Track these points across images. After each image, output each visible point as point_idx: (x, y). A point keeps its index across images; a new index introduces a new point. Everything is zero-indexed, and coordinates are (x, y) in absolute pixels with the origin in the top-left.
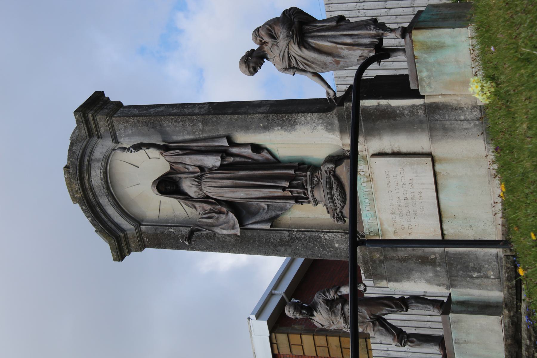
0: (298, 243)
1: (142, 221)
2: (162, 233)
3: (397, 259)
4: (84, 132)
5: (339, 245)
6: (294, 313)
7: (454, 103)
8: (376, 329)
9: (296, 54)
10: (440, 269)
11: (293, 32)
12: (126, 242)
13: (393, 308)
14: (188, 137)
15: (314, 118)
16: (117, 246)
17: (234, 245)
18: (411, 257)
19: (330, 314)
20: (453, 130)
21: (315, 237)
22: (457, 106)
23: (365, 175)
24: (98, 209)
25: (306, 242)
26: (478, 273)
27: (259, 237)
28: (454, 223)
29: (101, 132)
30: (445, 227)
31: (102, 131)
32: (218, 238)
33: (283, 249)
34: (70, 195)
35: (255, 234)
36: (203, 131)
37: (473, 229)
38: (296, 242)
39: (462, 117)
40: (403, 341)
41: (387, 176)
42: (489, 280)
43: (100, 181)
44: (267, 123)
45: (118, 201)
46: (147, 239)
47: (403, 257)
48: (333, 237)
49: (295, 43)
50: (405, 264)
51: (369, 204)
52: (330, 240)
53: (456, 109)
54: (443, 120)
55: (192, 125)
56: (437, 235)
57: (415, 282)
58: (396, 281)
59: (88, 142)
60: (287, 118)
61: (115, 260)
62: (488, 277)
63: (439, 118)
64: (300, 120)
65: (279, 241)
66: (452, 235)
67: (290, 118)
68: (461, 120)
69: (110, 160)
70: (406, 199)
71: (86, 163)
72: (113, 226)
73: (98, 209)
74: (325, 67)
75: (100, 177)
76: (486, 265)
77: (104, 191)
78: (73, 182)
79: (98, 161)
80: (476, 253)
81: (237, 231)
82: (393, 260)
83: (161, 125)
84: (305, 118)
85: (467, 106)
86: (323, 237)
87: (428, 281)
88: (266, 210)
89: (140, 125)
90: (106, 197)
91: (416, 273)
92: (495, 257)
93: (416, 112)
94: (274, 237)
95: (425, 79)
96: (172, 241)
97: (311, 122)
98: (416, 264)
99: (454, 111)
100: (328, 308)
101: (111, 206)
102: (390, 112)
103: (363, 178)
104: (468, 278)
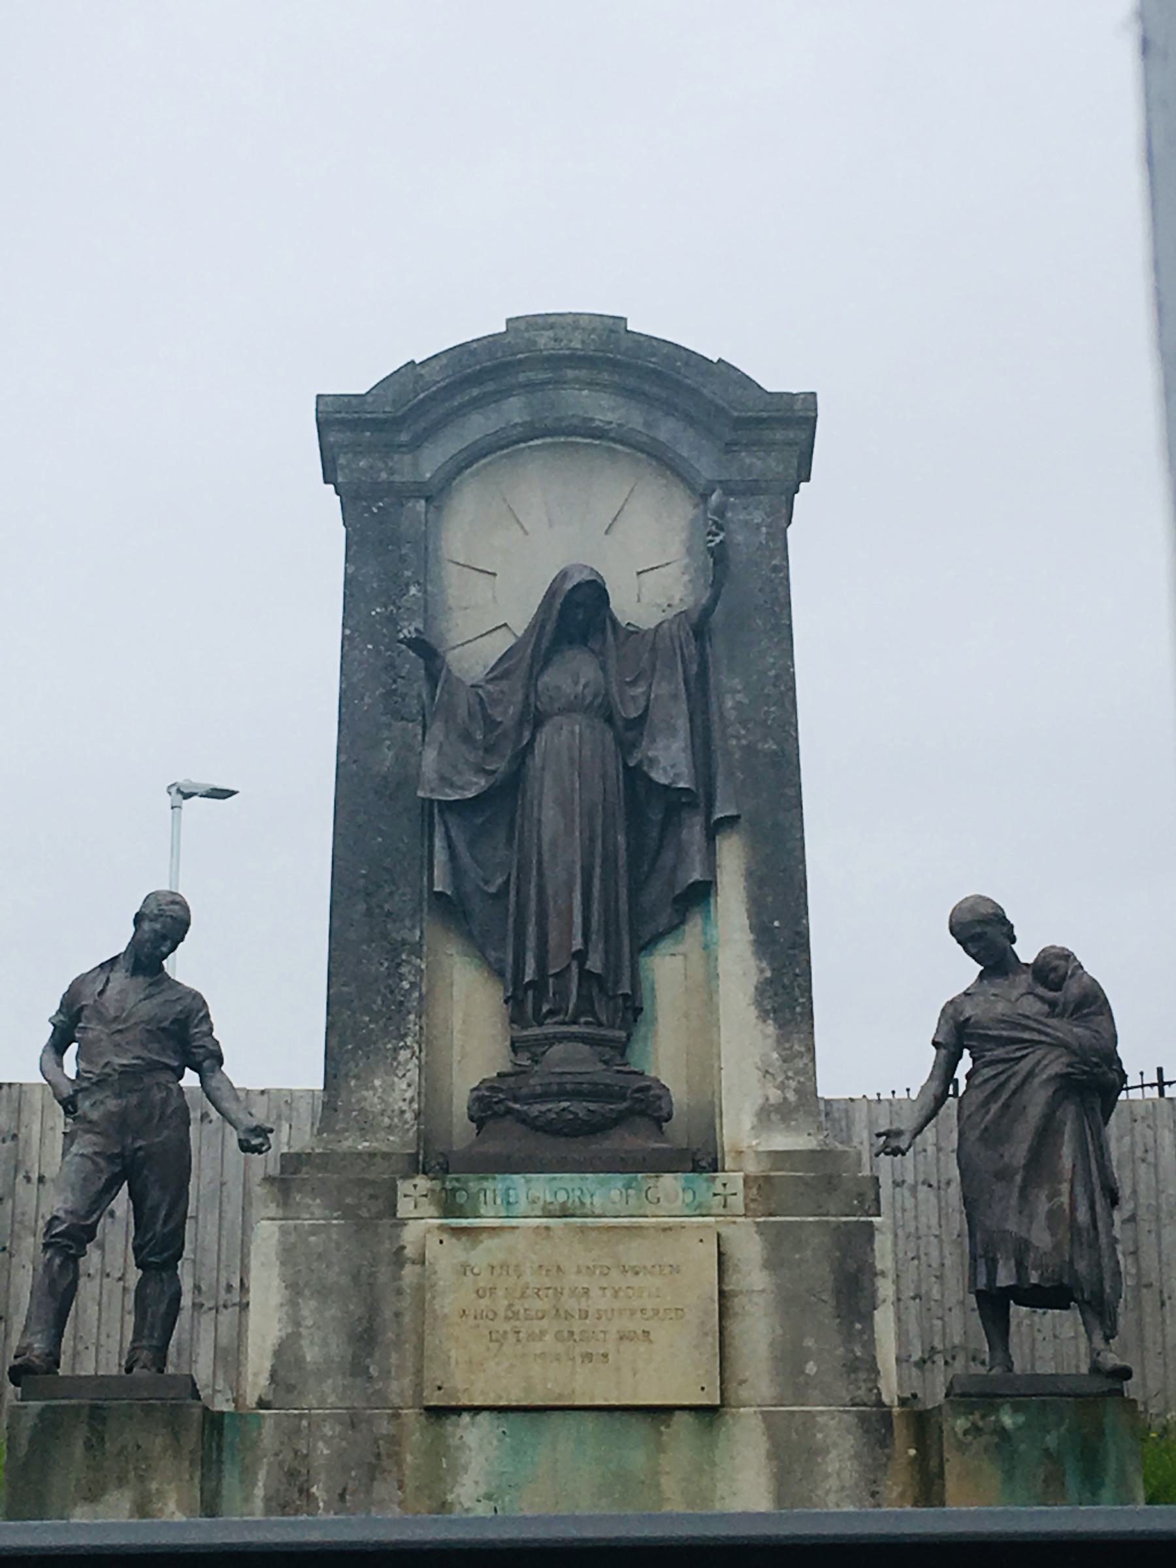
8: (102, 1163)
9: (1039, 1062)
13: (165, 1223)
19: (149, 1027)
29: (743, 454)
38: (382, 961)
46: (379, 508)
49: (1069, 1065)
60: (801, 1000)
65: (387, 907)
67: (798, 1009)
70: (585, 1315)
86: (402, 1044)
88: (486, 888)
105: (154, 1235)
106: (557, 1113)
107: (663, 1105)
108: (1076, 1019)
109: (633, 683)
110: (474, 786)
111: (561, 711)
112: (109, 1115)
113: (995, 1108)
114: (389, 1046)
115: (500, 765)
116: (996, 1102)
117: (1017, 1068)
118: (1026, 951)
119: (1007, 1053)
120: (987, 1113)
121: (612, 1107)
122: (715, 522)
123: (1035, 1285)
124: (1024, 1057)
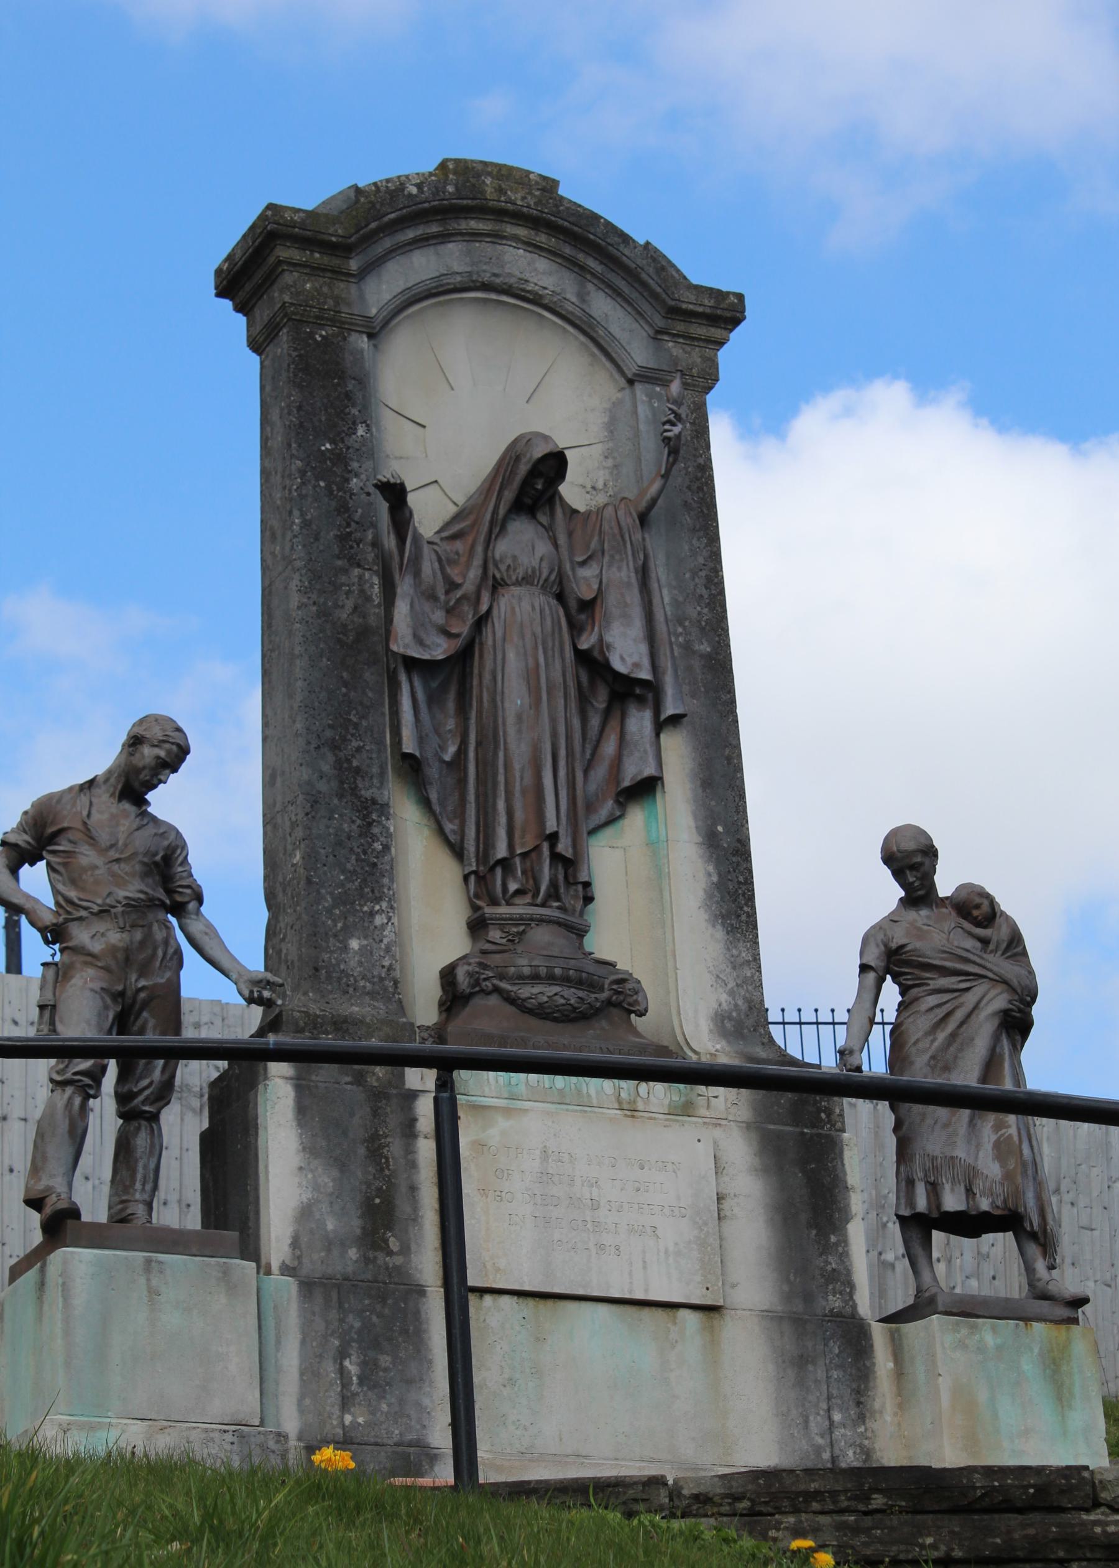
0: (353, 822)
1: (375, 346)
2: (348, 396)
3: (377, 1131)
4: (688, 301)
5: (356, 952)
6: (173, 743)
7: (874, 1400)
10: (354, 1258)
12: (324, 270)
15: (750, 988)
16: (326, 237)
17: (324, 614)
18: (388, 1176)
20: (801, 1383)
21: (377, 882)
22: (868, 1407)
23: (639, 1099)
24: (434, 228)
25: (357, 850)
26: (359, 1378)
27: (361, 703)
28: (519, 1332)
30: (506, 1301)
34: (472, 161)
35: (370, 694)
37: (505, 1386)
38: (354, 818)
39: (837, 1417)
40: (91, 1083)
41: (660, 1164)
42: (336, 1407)
44: (725, 845)
45: (442, 298)
47: (385, 1151)
48: (381, 941)
50: (362, 1151)
51: (547, 1086)
52: (372, 928)
53: (859, 1404)
54: (827, 1362)
55: (703, 623)
56: (486, 1275)
57: (301, 1168)
58: (301, 1110)
59: (655, 295)
62: (346, 1402)
63: (831, 1352)
65: (355, 763)
66: (482, 1320)
68: (829, 1410)
70: (595, 1206)
71: (581, 257)
73: (434, 228)
74: (935, 1066)
75: (531, 280)
76: (389, 1405)
77: (484, 271)
79: (582, 296)
80: (427, 1384)
81: (403, 642)
82: (374, 1116)
85: (869, 1434)
86: (377, 907)
87: (305, 1213)
89: (690, 469)
90: (469, 269)
91: (334, 1180)
92: (418, 1440)
93: (834, 1289)
94: (364, 755)
95: (977, 1337)
96: (323, 419)
97: (738, 976)
98: (364, 1187)
99: (854, 1396)
101: (437, 274)
102: (831, 1216)
103: (628, 1090)
104: (337, 1343)
105: (151, 1083)
106: (548, 997)
107: (639, 999)
108: (1007, 958)
109: (583, 564)
110: (439, 649)
111: (518, 583)
112: (113, 950)
113: (942, 1036)
114: (365, 909)
115: (463, 628)
116: (943, 1030)
117: (961, 1000)
118: (945, 884)
119: (953, 983)
120: (933, 1041)
121: (596, 995)
122: (673, 412)
123: (986, 1213)
124: (968, 989)
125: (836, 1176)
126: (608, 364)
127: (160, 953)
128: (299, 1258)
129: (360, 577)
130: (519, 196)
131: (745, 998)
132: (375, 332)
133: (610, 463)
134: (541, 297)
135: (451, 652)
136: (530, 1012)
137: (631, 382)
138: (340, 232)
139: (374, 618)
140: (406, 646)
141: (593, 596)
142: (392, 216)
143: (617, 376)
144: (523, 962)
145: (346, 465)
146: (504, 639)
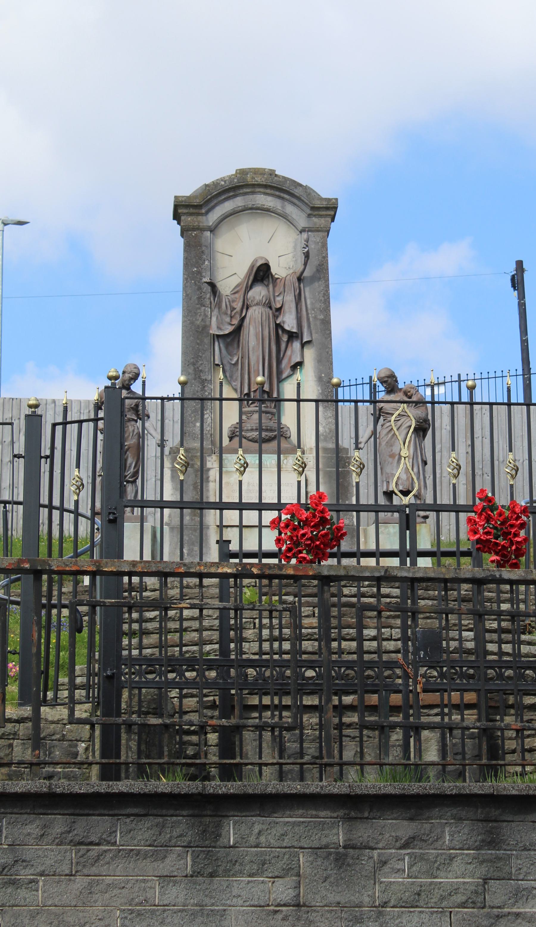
1: (213, 234)
2: (203, 252)
4: (318, 204)
11: (422, 422)
14: (309, 302)
17: (192, 323)
24: (231, 194)
27: (203, 350)
31: (315, 220)
32: (200, 308)
33: (191, 371)
36: (315, 318)
43: (261, 203)
50: (191, 488)
57: (172, 494)
59: (306, 204)
61: (176, 197)
64: (328, 412)
65: (200, 368)
69: (281, 218)
72: (212, 204)
73: (231, 194)
78: (263, 177)
79: (283, 207)
81: (214, 330)
83: (320, 278)
84: (330, 417)
94: (203, 365)
100: (132, 406)
109: (278, 296)
111: (255, 305)
115: (236, 322)
124: (399, 420)
125: (349, 483)
126: (293, 227)
127: (131, 435)
128: (171, 520)
129: (204, 310)
130: (259, 179)
131: (329, 429)
132: (213, 230)
133: (294, 259)
134: (269, 209)
135: (231, 330)
136: (250, 440)
137: (301, 232)
138: (198, 201)
139: (208, 323)
140: (215, 331)
141: (280, 306)
142: (215, 193)
143: (296, 230)
144: (248, 425)
145: (201, 274)
146: (249, 324)
